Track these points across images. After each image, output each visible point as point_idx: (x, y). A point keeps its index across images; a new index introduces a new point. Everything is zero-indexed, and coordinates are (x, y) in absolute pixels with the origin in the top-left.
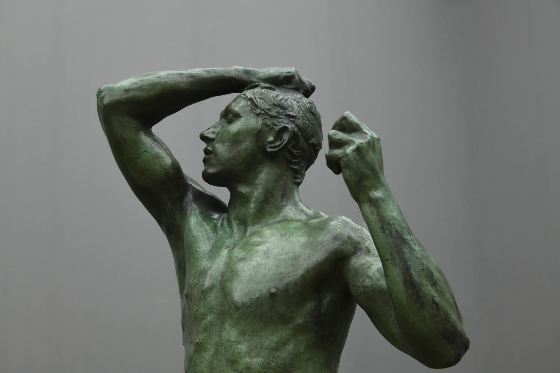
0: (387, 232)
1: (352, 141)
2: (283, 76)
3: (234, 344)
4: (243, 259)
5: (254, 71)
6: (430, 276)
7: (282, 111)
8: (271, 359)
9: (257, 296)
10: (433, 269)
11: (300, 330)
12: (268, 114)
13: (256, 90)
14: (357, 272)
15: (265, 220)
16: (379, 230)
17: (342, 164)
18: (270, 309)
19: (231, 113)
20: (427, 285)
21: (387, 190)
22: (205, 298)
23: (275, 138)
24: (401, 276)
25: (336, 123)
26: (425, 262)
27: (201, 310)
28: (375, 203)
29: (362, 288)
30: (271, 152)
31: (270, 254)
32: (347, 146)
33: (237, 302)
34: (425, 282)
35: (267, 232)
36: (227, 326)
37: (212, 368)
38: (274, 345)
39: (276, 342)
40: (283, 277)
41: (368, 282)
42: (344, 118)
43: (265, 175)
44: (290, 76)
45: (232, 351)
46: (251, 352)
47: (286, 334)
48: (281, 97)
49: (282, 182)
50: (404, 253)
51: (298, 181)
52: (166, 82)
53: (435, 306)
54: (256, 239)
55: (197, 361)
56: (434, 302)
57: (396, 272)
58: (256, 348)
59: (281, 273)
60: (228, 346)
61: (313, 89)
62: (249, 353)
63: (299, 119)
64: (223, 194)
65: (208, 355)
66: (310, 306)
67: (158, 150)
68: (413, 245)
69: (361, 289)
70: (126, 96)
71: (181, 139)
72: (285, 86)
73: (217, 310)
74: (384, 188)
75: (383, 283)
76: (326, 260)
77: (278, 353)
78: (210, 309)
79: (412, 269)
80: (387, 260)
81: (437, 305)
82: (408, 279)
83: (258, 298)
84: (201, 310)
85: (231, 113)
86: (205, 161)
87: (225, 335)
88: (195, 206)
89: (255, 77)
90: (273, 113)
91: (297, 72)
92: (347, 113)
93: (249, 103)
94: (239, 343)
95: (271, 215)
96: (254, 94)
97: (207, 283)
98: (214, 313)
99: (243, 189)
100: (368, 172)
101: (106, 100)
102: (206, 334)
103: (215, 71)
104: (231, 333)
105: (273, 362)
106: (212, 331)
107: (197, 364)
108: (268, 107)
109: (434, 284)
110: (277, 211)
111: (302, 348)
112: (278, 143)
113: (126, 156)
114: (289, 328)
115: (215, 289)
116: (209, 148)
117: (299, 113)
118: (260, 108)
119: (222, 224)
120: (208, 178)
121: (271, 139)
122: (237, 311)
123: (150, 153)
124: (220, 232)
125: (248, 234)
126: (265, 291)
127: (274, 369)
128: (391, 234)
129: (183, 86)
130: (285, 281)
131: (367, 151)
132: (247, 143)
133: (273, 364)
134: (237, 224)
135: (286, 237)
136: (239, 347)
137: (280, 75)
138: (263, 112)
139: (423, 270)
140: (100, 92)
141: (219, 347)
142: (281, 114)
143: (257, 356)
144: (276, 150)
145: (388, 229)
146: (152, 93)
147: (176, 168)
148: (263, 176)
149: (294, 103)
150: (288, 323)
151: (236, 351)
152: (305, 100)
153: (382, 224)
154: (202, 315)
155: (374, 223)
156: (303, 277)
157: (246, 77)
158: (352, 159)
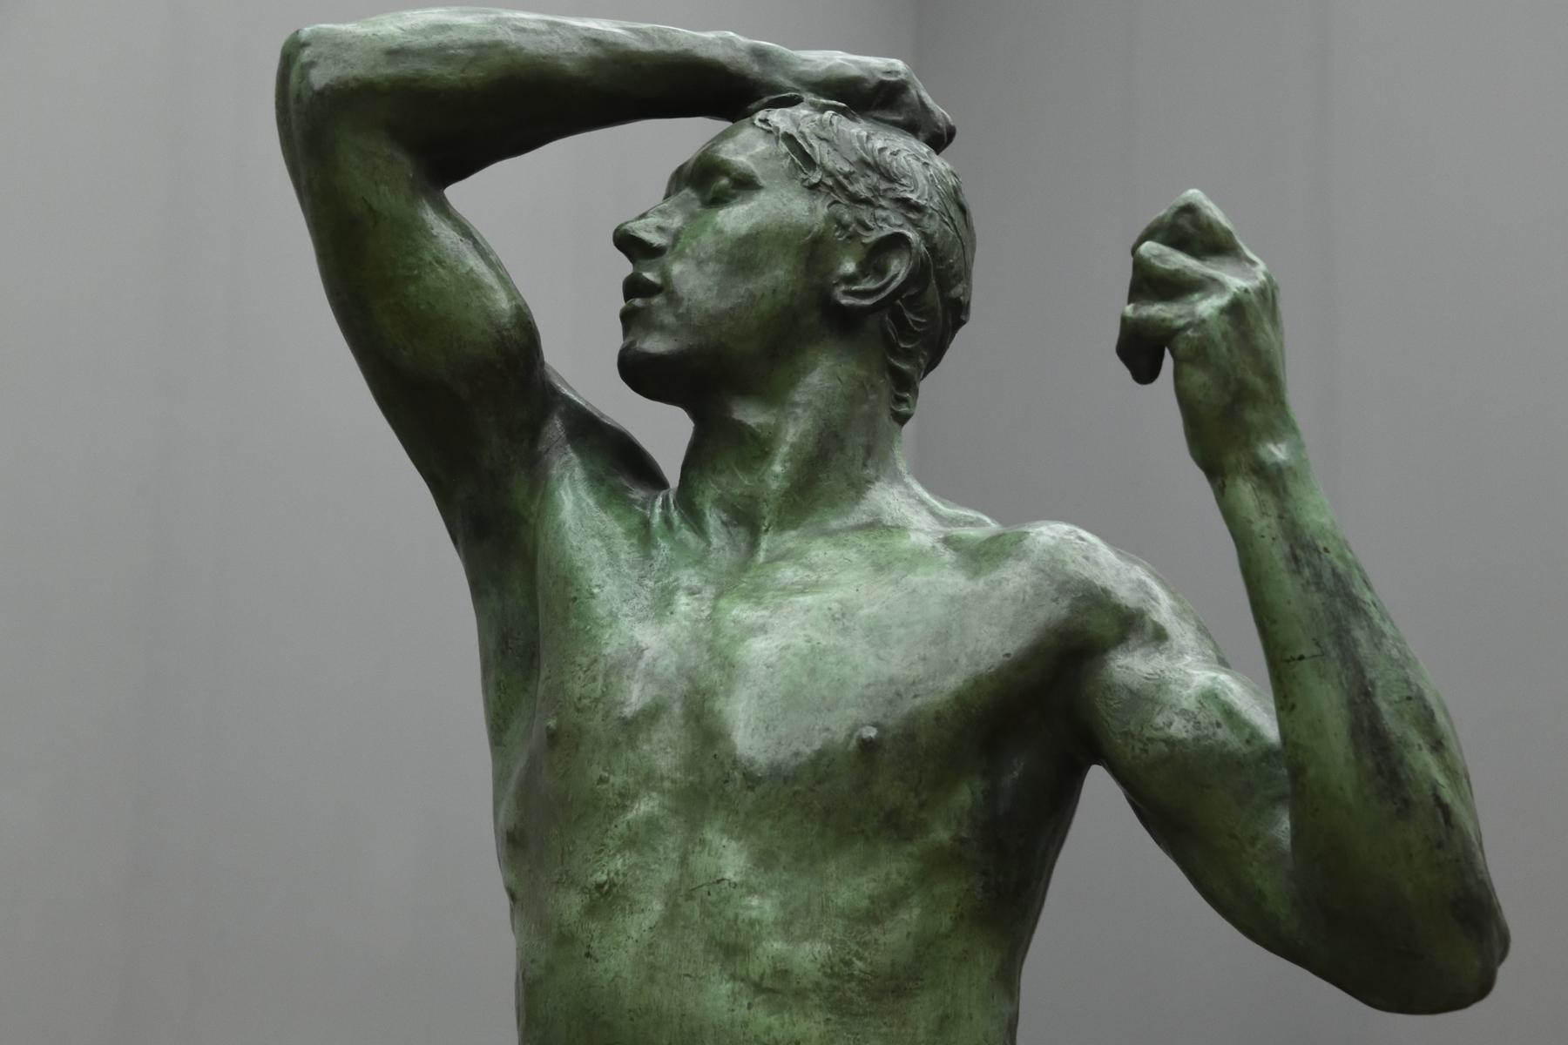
0: (1307, 572)
1: (1214, 280)
2: (873, 82)
3: (736, 893)
5: (781, 55)
7: (884, 185)
8: (855, 948)
9: (817, 745)
11: (939, 863)
12: (844, 188)
15: (816, 519)
16: (1282, 565)
18: (853, 792)
19: (726, 173)
20: (1420, 748)
21: (1298, 447)
22: (632, 743)
24: (1344, 712)
25: (1160, 221)
28: (1272, 480)
29: (1162, 745)
30: (851, 307)
32: (1197, 296)
33: (752, 761)
34: (1415, 737)
35: (820, 551)
36: (712, 835)
37: (652, 967)
39: (870, 897)
40: (898, 694)
41: (1179, 729)
42: (1189, 209)
43: (822, 378)
44: (896, 83)
45: (730, 914)
46: (791, 923)
47: (899, 873)
48: (878, 144)
49: (866, 407)
51: (904, 409)
53: (1440, 814)
55: (594, 945)
56: (1438, 800)
57: (1327, 700)
58: (808, 911)
60: (714, 898)
61: (951, 133)
62: (786, 926)
67: (474, 262)
71: (541, 240)
72: (877, 114)
73: (674, 781)
76: (1035, 653)
77: (876, 931)
79: (1379, 692)
80: (1301, 658)
82: (1366, 724)
84: (617, 780)
87: (701, 862)
88: (572, 455)
89: (786, 75)
90: (860, 188)
92: (1194, 194)
93: (784, 148)
94: (752, 891)
95: (833, 505)
96: (796, 123)
97: (635, 697)
98: (662, 792)
99: (751, 415)
100: (1259, 383)
101: (320, 78)
102: (632, 857)
103: (663, 36)
104: (730, 858)
105: (860, 958)
106: (654, 849)
108: (847, 168)
110: (852, 493)
111: (945, 921)
112: (868, 284)
114: (911, 855)
115: (665, 719)
116: (649, 276)
119: (667, 520)
121: (849, 267)
122: (752, 789)
123: (452, 270)
125: (761, 556)
127: (861, 981)
129: (569, 65)
130: (907, 706)
132: (779, 273)
133: (859, 964)
134: (724, 524)
135: (894, 576)
136: (755, 902)
137: (865, 75)
138: (830, 182)
139: (1409, 698)
141: (681, 900)
143: (812, 935)
144: (867, 302)
145: (1309, 564)
146: (476, 74)
149: (916, 165)
150: (909, 839)
151: (745, 915)
153: (1291, 547)
154: (621, 795)
155: (1268, 540)
156: (959, 698)
157: (756, 68)
158: (1217, 336)
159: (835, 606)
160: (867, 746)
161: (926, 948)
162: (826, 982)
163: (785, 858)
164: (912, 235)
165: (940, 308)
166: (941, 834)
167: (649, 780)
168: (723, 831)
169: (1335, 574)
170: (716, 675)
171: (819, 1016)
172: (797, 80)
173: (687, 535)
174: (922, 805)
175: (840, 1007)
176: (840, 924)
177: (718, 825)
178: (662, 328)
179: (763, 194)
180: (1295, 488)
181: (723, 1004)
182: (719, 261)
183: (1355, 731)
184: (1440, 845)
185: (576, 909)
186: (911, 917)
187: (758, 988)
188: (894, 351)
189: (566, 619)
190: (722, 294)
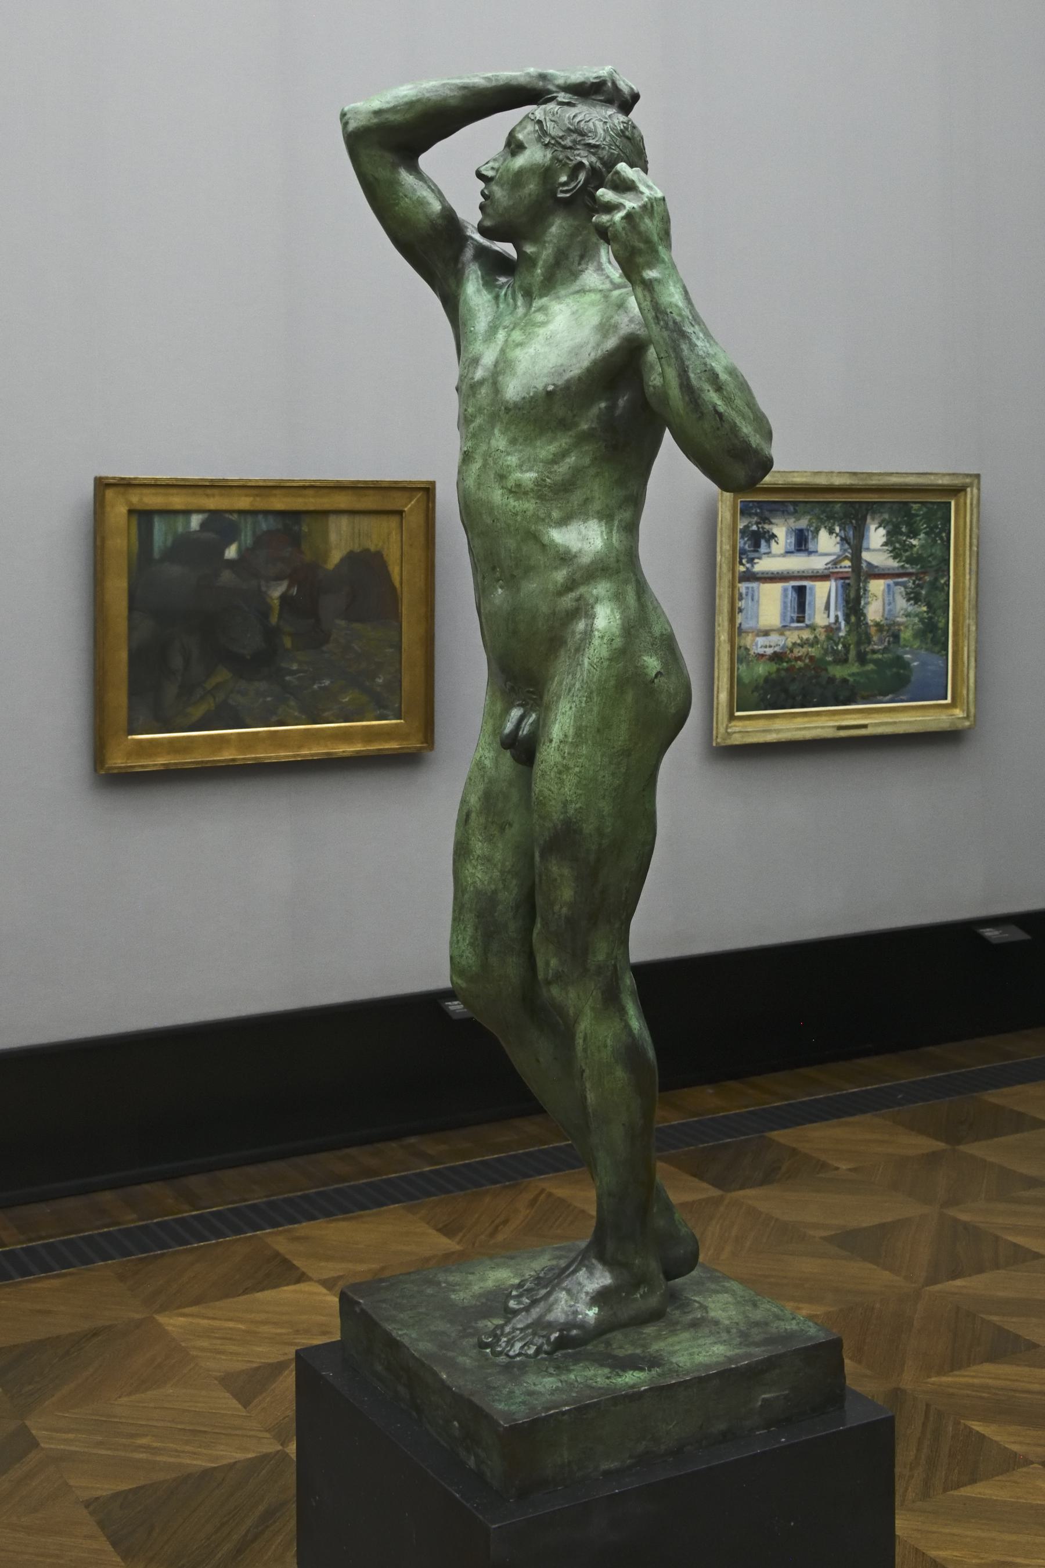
0: (662, 323)
3: (503, 455)
4: (520, 345)
5: (552, 75)
6: (713, 378)
7: (579, 138)
10: (719, 369)
13: (552, 106)
18: (547, 412)
22: (474, 395)
23: (569, 177)
26: (708, 360)
31: (561, 333)
33: (507, 402)
34: (707, 386)
38: (551, 457)
43: (557, 227)
49: (580, 238)
50: (682, 350)
52: (429, 99)
54: (540, 317)
56: (716, 412)
59: (562, 365)
61: (635, 97)
62: (520, 466)
63: (604, 148)
64: (508, 249)
65: (475, 466)
68: (694, 339)
70: (375, 121)
74: (662, 265)
77: (556, 467)
81: (720, 415)
83: (532, 398)
86: (482, 207)
90: (568, 142)
91: (611, 75)
94: (508, 454)
95: (563, 284)
100: (642, 246)
101: (352, 126)
103: (497, 77)
104: (499, 441)
109: (719, 388)
111: (587, 461)
112: (573, 185)
118: (550, 135)
119: (506, 295)
120: (482, 230)
123: (411, 199)
124: (502, 306)
126: (540, 386)
128: (666, 327)
129: (453, 102)
130: (567, 376)
136: (509, 458)
140: (343, 115)
142: (579, 143)
143: (530, 470)
144: (568, 195)
147: (449, 217)
148: (554, 229)
150: (569, 430)
152: (622, 118)
156: (589, 371)
158: (620, 229)
160: (549, 394)
161: (577, 472)
163: (521, 440)
166: (585, 426)
169: (675, 322)
171: (533, 501)
175: (541, 497)
180: (657, 288)
181: (499, 498)
183: (681, 386)
184: (718, 429)
187: (511, 491)
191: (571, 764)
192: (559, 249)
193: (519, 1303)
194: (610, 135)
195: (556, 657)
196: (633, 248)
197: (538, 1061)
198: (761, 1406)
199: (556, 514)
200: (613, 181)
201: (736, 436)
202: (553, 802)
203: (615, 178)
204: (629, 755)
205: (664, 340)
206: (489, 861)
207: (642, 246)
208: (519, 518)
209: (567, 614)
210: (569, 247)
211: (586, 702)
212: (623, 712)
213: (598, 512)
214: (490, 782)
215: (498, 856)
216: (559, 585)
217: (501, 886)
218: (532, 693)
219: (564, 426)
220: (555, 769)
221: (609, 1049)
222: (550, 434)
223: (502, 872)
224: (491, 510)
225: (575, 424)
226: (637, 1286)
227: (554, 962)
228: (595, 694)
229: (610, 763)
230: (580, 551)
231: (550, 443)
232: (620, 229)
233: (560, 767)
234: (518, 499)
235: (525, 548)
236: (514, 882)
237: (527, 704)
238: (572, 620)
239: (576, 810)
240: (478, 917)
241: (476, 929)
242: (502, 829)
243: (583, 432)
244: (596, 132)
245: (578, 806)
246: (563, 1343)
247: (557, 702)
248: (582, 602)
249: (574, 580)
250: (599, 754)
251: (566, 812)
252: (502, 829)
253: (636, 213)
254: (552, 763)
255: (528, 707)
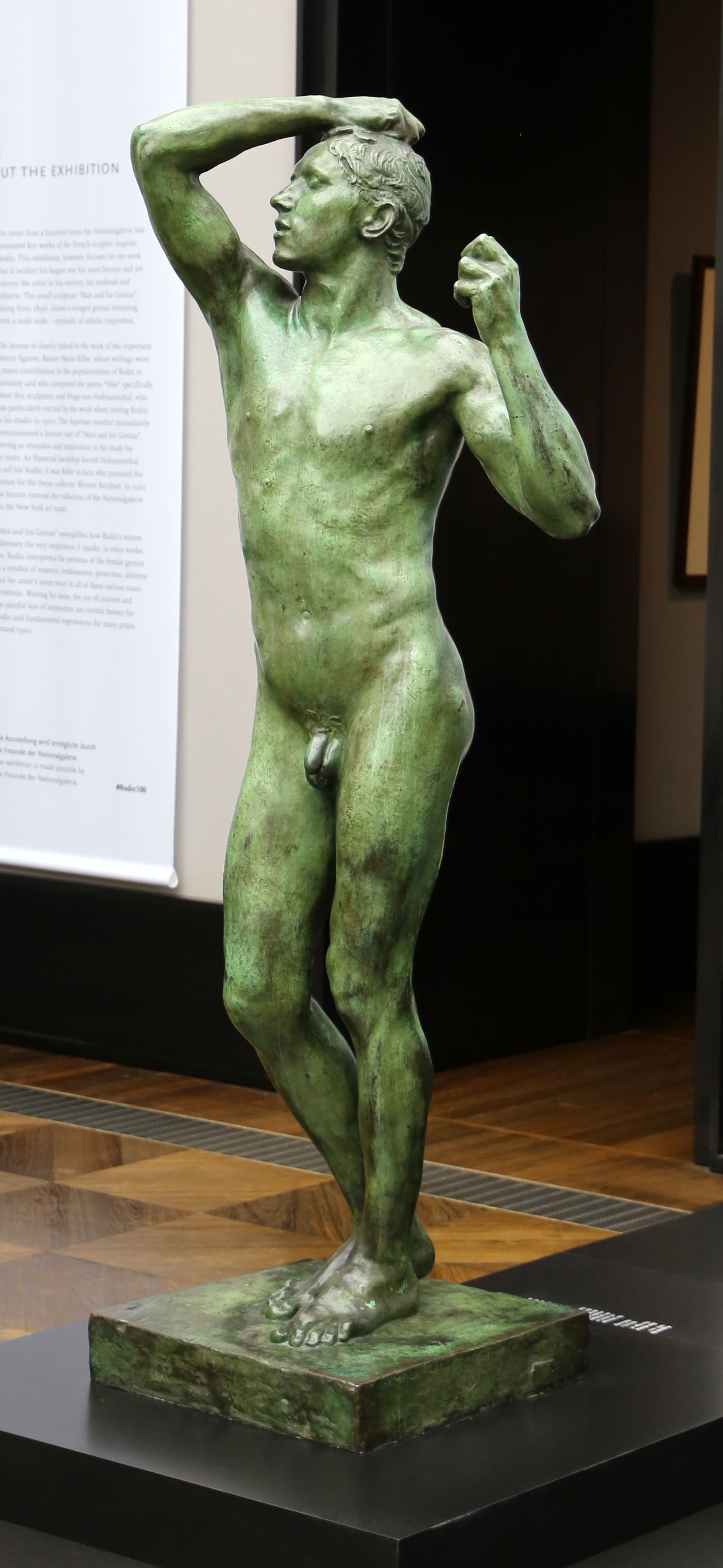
0: (519, 385)
1: (487, 274)
3: (318, 490)
9: (349, 433)
14: (474, 414)
17: (474, 302)
19: (317, 176)
22: (278, 427)
27: (273, 442)
33: (324, 439)
34: (557, 445)
37: (287, 516)
38: (367, 494)
41: (487, 430)
56: (565, 468)
62: (336, 503)
64: (288, 276)
66: (411, 448)
69: (478, 437)
72: (386, 133)
75: (506, 433)
76: (437, 393)
77: (372, 505)
78: (285, 442)
81: (568, 472)
83: (350, 436)
84: (273, 442)
85: (317, 176)
87: (305, 477)
89: (346, 116)
93: (341, 165)
94: (324, 490)
95: (362, 320)
97: (280, 407)
98: (290, 447)
100: (503, 314)
101: (149, 148)
107: (267, 509)
108: (368, 174)
111: (400, 498)
113: (167, 222)
117: (406, 180)
120: (279, 261)
125: (332, 344)
131: (504, 288)
133: (365, 517)
136: (325, 494)
143: (347, 506)
144: (376, 235)
150: (385, 468)
156: (407, 414)
159: (359, 372)
160: (369, 434)
161: (392, 509)
162: (352, 524)
163: (336, 477)
164: (393, 204)
165: (411, 225)
166: (399, 466)
167: (285, 443)
168: (313, 466)
169: (530, 385)
170: (311, 400)
171: (349, 536)
172: (351, 119)
173: (301, 330)
174: (390, 455)
175: (357, 533)
176: (358, 501)
177: (311, 462)
178: (290, 247)
179: (332, 187)
182: (313, 218)
184: (565, 484)
185: (259, 491)
186: (386, 499)
187: (326, 526)
188: (390, 247)
189: (253, 369)
190: (314, 233)
191: (391, 789)
192: (360, 285)
193: (283, 1309)
194: (411, 177)
195: (370, 687)
196: (496, 315)
197: (307, 1076)
198: (535, 1373)
199: (371, 550)
200: (475, 250)
201: (579, 490)
202: (372, 824)
203: (479, 248)
204: (438, 779)
205: (522, 400)
206: (272, 883)
207: (503, 314)
208: (334, 552)
209: (384, 646)
210: (368, 283)
211: (406, 730)
212: (437, 738)
213: (409, 548)
214: (273, 806)
215: (282, 879)
216: (376, 618)
217: (285, 907)
218: (337, 720)
219: (381, 464)
220: (375, 793)
221: (401, 1056)
222: (366, 471)
223: (287, 894)
224: (301, 544)
225: (390, 463)
226: (400, 1282)
227: (356, 977)
228: (414, 723)
229: (425, 787)
230: (397, 584)
231: (367, 479)
232: (487, 298)
233: (380, 791)
234: (334, 534)
235: (338, 581)
236: (299, 903)
237: (330, 731)
238: (388, 651)
239: (394, 831)
240: (263, 938)
241: (261, 949)
242: (287, 852)
243: (398, 472)
244: (398, 173)
245: (397, 826)
246: (356, 1331)
247: (374, 730)
248: (398, 635)
249: (391, 614)
250: (416, 779)
251: (384, 834)
252: (287, 852)
253: (501, 284)
254: (372, 788)
255: (332, 734)
